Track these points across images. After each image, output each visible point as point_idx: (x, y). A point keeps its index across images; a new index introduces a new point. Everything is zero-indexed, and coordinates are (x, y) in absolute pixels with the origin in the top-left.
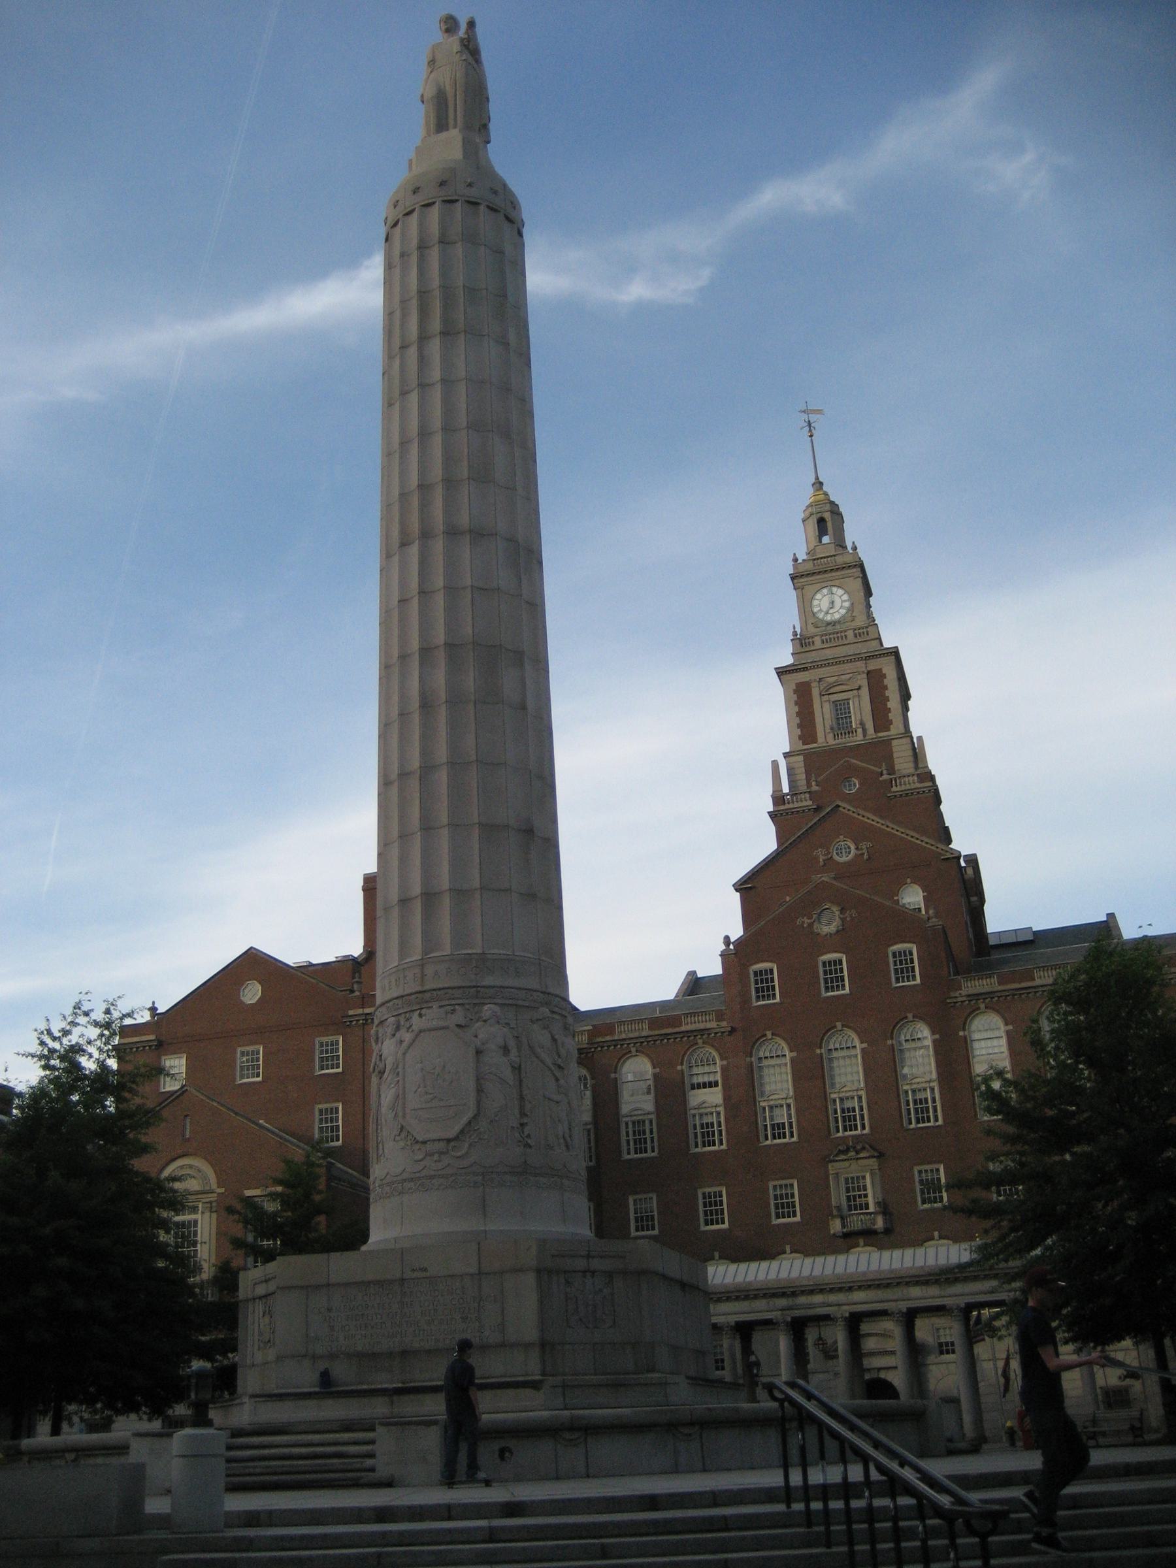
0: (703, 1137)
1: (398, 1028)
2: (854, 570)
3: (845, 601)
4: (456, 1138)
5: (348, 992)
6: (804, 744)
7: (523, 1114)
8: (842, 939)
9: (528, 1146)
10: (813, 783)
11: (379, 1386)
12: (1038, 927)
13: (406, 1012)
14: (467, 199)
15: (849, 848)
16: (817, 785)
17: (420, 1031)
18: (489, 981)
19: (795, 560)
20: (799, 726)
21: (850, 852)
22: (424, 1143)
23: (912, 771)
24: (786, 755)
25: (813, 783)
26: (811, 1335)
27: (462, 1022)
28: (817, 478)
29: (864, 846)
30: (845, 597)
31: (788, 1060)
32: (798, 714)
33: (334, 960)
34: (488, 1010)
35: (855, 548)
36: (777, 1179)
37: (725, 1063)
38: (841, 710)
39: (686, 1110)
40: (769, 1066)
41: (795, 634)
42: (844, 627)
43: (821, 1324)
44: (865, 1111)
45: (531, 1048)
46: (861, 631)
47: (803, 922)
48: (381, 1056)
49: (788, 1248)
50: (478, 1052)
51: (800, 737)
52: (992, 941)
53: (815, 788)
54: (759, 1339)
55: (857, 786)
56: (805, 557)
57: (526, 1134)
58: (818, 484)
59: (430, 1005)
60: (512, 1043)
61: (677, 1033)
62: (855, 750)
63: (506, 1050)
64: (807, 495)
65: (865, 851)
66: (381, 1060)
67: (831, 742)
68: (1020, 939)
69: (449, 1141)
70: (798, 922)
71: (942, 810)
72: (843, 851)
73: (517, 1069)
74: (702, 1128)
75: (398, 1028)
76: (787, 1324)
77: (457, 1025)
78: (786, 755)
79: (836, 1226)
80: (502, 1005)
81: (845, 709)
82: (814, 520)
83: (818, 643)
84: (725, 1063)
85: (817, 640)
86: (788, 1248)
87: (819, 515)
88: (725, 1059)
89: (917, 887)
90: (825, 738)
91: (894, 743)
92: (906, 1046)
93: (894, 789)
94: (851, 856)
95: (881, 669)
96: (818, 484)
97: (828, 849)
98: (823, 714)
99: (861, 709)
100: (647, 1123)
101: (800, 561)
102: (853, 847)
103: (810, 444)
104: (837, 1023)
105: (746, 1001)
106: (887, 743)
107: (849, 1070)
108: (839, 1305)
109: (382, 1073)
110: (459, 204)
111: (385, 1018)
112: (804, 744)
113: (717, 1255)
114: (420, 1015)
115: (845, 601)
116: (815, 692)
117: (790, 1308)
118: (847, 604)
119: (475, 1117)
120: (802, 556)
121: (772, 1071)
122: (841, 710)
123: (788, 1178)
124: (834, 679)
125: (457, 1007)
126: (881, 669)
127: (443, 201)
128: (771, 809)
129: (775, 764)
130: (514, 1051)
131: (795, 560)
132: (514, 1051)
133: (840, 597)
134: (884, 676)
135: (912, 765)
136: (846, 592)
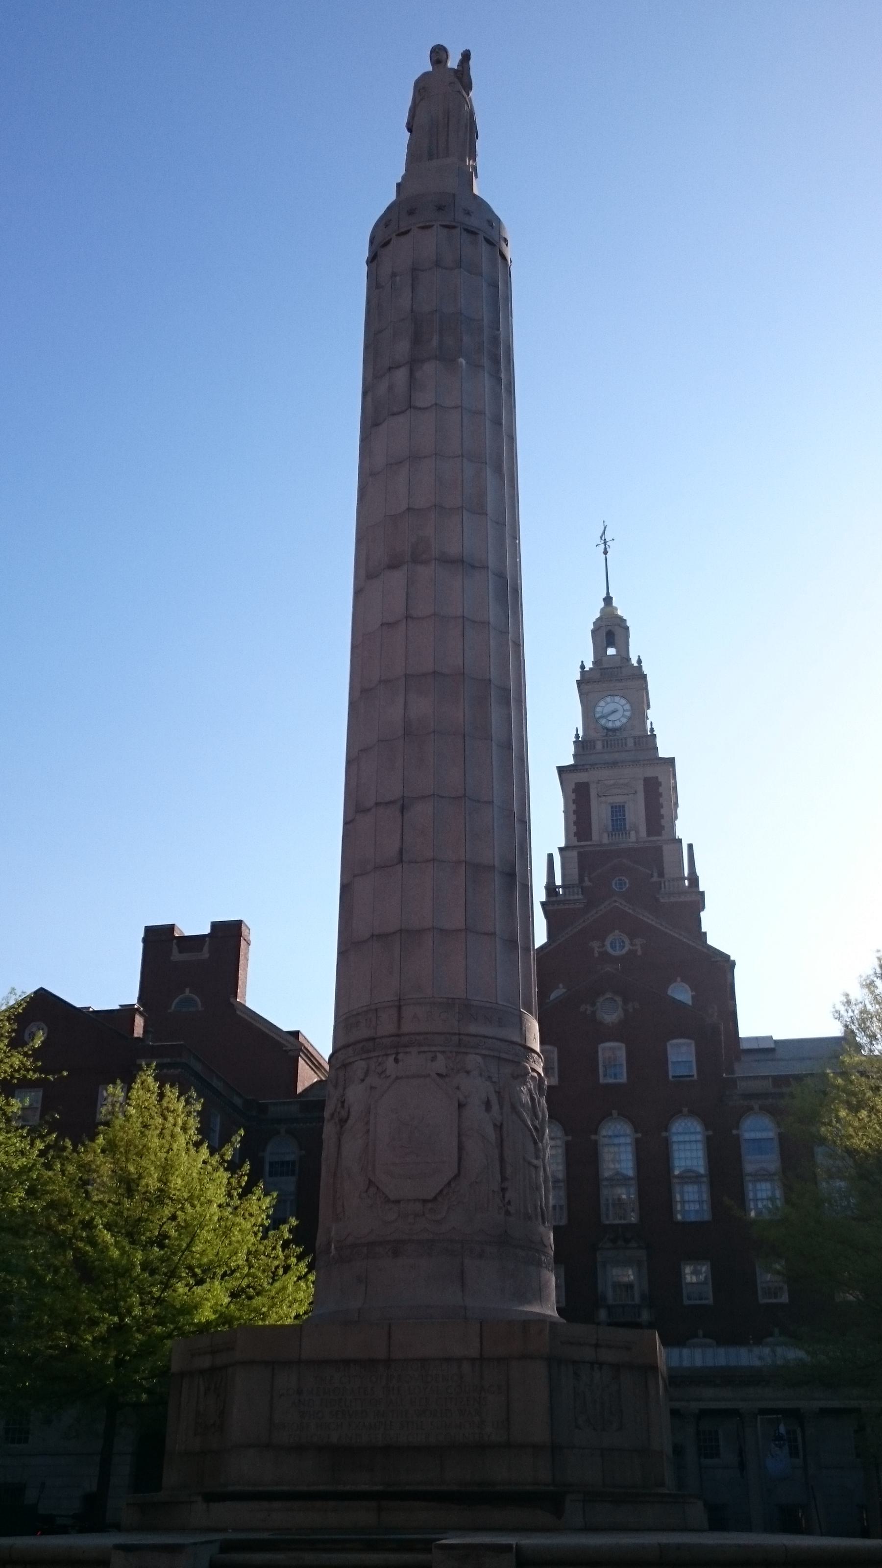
1: (367, 1074)
3: (627, 711)
4: (435, 1199)
6: (578, 841)
7: (504, 1179)
9: (508, 1213)
11: (348, 1488)
12: (779, 1035)
13: (379, 1056)
14: (466, 227)
15: (623, 942)
16: (590, 881)
17: (397, 1078)
18: (473, 1029)
19: (583, 667)
20: (575, 823)
21: (624, 947)
22: (398, 1202)
24: (561, 850)
25: (586, 879)
27: (443, 1071)
28: (608, 593)
29: (638, 941)
30: (627, 707)
32: (575, 812)
33: (118, 1008)
34: (473, 1060)
35: (639, 661)
38: (618, 811)
40: (679, 1142)
41: (577, 736)
45: (514, 1108)
47: (586, 1009)
48: (343, 1102)
50: (461, 1106)
51: (576, 834)
52: (744, 1046)
53: (587, 883)
55: (627, 886)
56: (591, 666)
57: (506, 1200)
58: (608, 600)
59: (408, 1050)
60: (494, 1099)
63: (488, 1105)
64: (595, 611)
66: (343, 1106)
67: (605, 841)
68: (761, 1046)
69: (425, 1201)
70: (582, 1008)
71: (701, 916)
73: (499, 1127)
75: (367, 1074)
77: (438, 1074)
78: (561, 850)
80: (484, 1056)
82: (603, 632)
83: (599, 746)
87: (609, 628)
89: (687, 986)
90: (599, 834)
92: (606, 1141)
94: (624, 951)
96: (608, 600)
98: (600, 814)
99: (636, 813)
101: (587, 669)
102: (627, 941)
103: (604, 561)
107: (688, 1154)
109: (343, 1121)
110: (457, 231)
111: (351, 1060)
112: (578, 841)
114: (396, 1061)
115: (627, 711)
116: (593, 792)
118: (628, 714)
119: (457, 1176)
120: (589, 665)
121: (682, 1146)
122: (618, 811)
124: (612, 782)
125: (438, 1055)
127: (419, 228)
128: (544, 900)
129: (550, 857)
130: (495, 1107)
131: (583, 667)
132: (495, 1107)
133: (622, 706)
136: (629, 702)
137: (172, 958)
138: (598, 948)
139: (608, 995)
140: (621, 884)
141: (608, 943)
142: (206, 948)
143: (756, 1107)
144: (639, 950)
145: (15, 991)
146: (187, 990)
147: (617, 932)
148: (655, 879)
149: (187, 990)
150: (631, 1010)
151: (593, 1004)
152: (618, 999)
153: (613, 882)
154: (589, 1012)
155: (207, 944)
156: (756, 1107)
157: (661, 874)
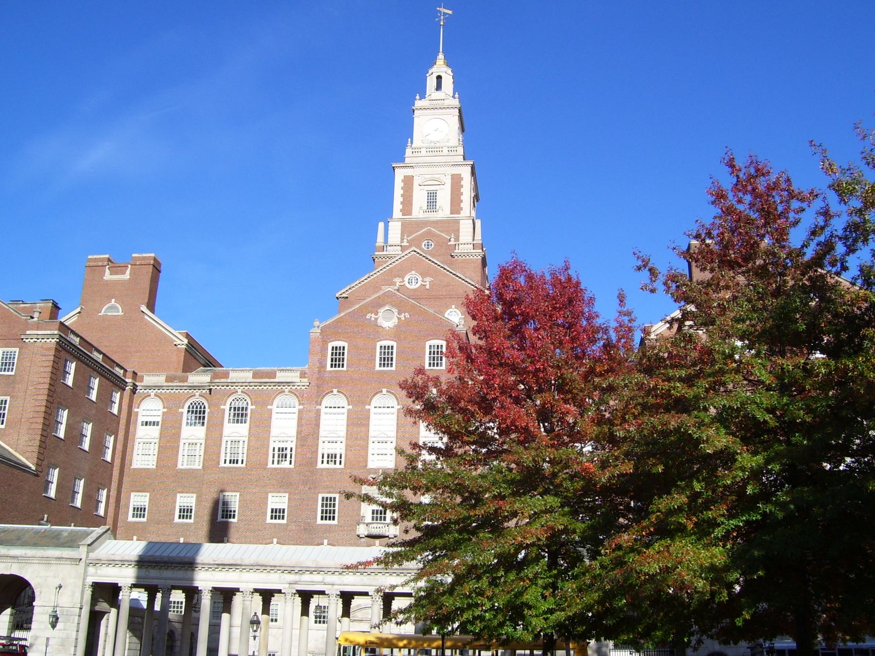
0: (279, 457)
2: (454, 110)
5: (29, 318)
6: (403, 215)
8: (397, 333)
10: (405, 240)
15: (417, 279)
21: (417, 283)
23: (471, 241)
26: (314, 602)
29: (428, 279)
31: (345, 411)
36: (324, 493)
37: (301, 407)
39: (221, 437)
42: (442, 145)
43: (701, 590)
44: (293, 453)
46: (452, 149)
47: (371, 317)
49: (326, 542)
54: (276, 601)
61: (271, 382)
62: (436, 223)
65: (428, 283)
70: (368, 316)
72: (413, 281)
74: (279, 451)
76: (384, 593)
79: (362, 530)
81: (431, 196)
84: (301, 407)
85: (423, 151)
86: (326, 542)
88: (303, 404)
91: (461, 222)
93: (456, 251)
95: (460, 174)
97: (403, 278)
100: (241, 443)
102: (420, 279)
104: (383, 390)
105: (323, 366)
106: (457, 222)
108: (333, 585)
112: (403, 215)
113: (275, 540)
116: (416, 183)
117: (296, 583)
123: (333, 493)
126: (460, 174)
134: (462, 179)
135: (471, 238)
137: (104, 278)
138: (399, 282)
139: (387, 308)
140: (428, 245)
141: (406, 279)
142: (128, 272)
143: (153, 394)
144: (428, 285)
145: (673, 300)
146: (113, 300)
147: (413, 272)
148: (452, 243)
149: (113, 300)
150: (403, 319)
151: (377, 314)
152: (395, 311)
153: (423, 244)
154: (373, 319)
155: (129, 269)
156: (153, 394)
157: (457, 239)
